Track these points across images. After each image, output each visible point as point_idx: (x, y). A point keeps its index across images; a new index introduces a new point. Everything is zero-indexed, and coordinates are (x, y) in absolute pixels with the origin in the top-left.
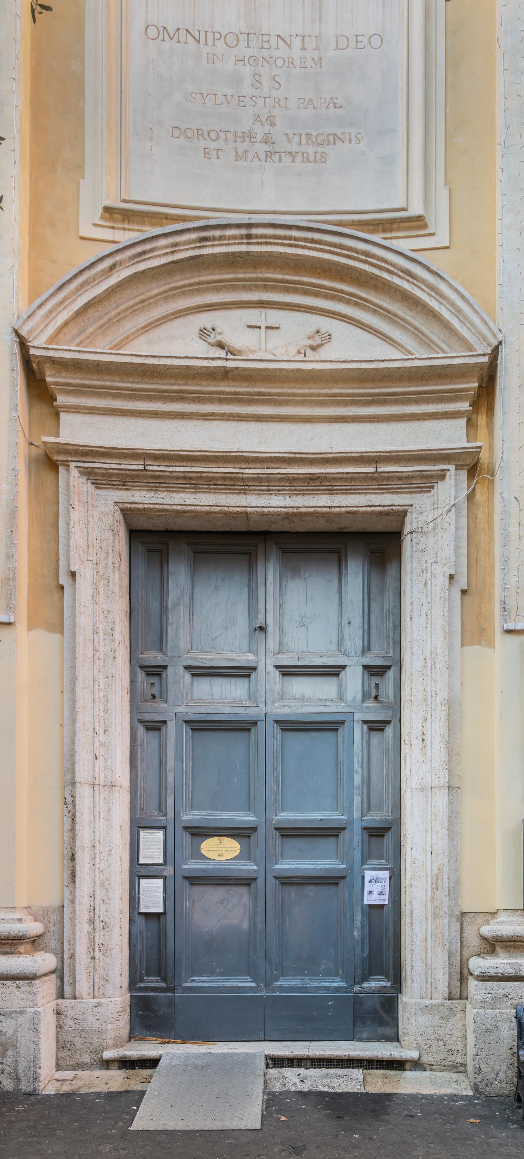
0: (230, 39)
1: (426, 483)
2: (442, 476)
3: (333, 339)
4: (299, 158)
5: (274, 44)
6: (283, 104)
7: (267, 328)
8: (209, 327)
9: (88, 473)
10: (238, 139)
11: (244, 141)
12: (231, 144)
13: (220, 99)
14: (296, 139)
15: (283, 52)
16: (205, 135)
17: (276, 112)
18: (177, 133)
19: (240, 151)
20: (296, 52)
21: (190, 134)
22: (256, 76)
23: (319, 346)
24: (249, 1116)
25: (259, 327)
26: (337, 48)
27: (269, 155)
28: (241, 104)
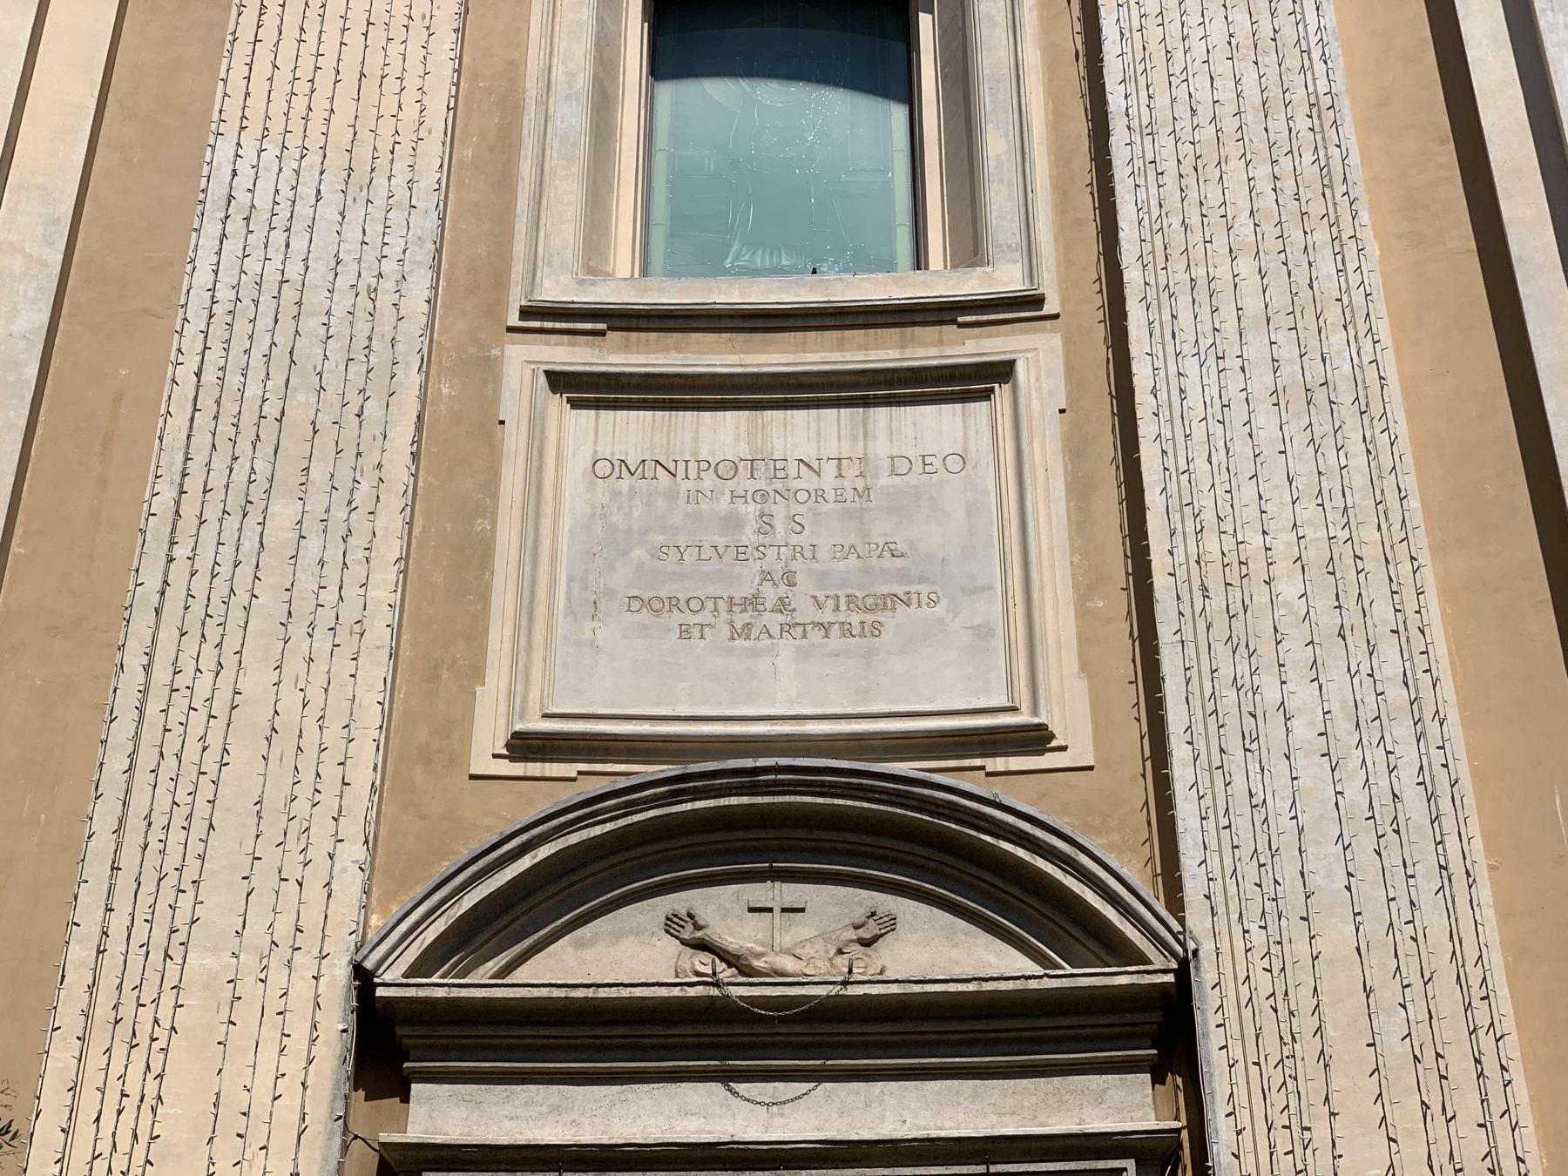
3: (898, 926)
4: (835, 630)
5: (793, 472)
6: (808, 554)
7: (784, 910)
8: (683, 912)
10: (735, 609)
11: (745, 610)
12: (724, 616)
13: (707, 552)
14: (830, 603)
15: (808, 481)
16: (682, 605)
17: (794, 566)
18: (636, 605)
19: (738, 625)
20: (828, 479)
21: (657, 605)
22: (765, 522)
23: (875, 939)
25: (770, 910)
26: (894, 473)
27: (786, 628)
28: (741, 557)
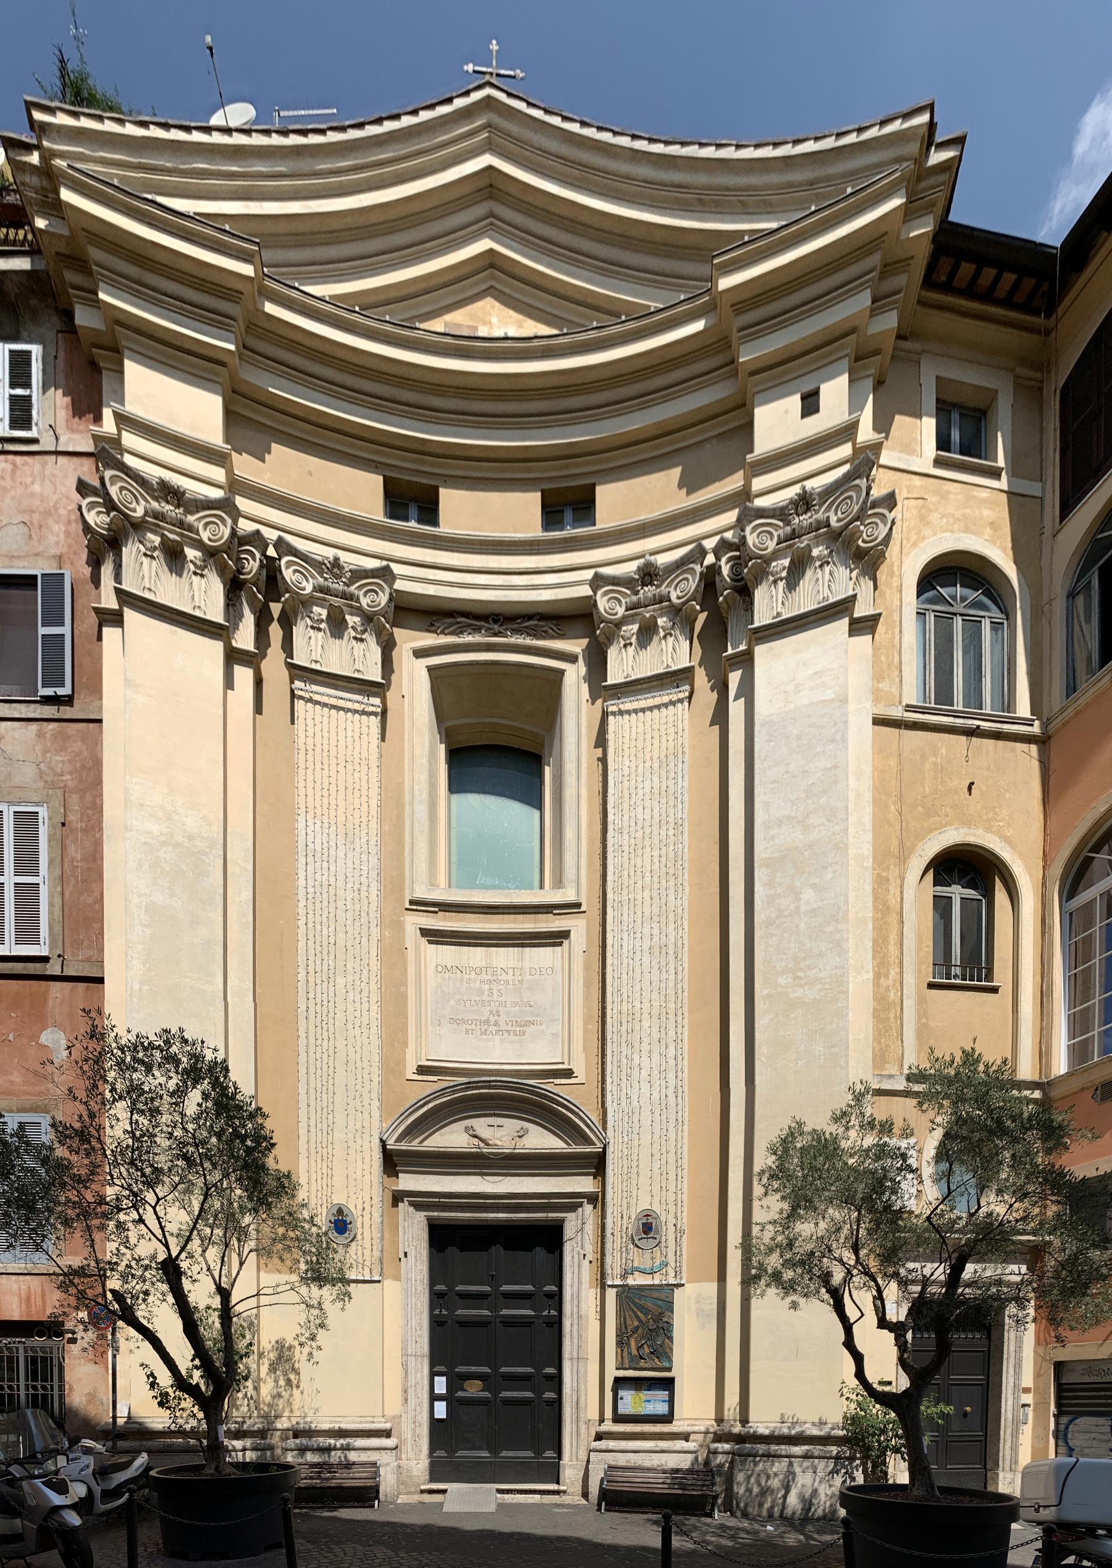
0: (478, 970)
1: (573, 1208)
2: (581, 1205)
9: (411, 1204)
13: (473, 1003)
15: (504, 977)
17: (500, 1009)
20: (510, 977)
24: (492, 1508)
27: (497, 1031)
